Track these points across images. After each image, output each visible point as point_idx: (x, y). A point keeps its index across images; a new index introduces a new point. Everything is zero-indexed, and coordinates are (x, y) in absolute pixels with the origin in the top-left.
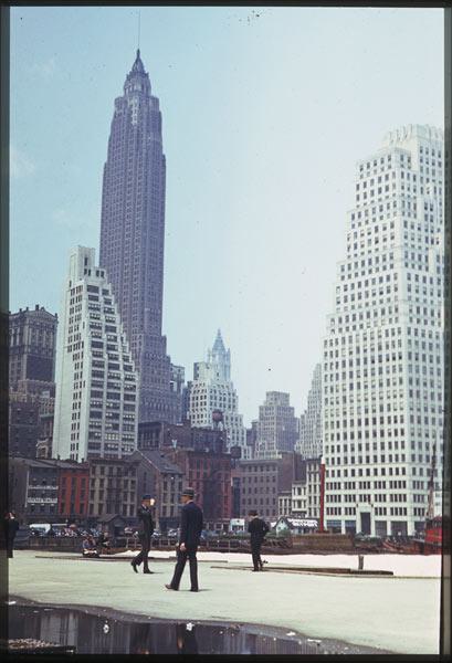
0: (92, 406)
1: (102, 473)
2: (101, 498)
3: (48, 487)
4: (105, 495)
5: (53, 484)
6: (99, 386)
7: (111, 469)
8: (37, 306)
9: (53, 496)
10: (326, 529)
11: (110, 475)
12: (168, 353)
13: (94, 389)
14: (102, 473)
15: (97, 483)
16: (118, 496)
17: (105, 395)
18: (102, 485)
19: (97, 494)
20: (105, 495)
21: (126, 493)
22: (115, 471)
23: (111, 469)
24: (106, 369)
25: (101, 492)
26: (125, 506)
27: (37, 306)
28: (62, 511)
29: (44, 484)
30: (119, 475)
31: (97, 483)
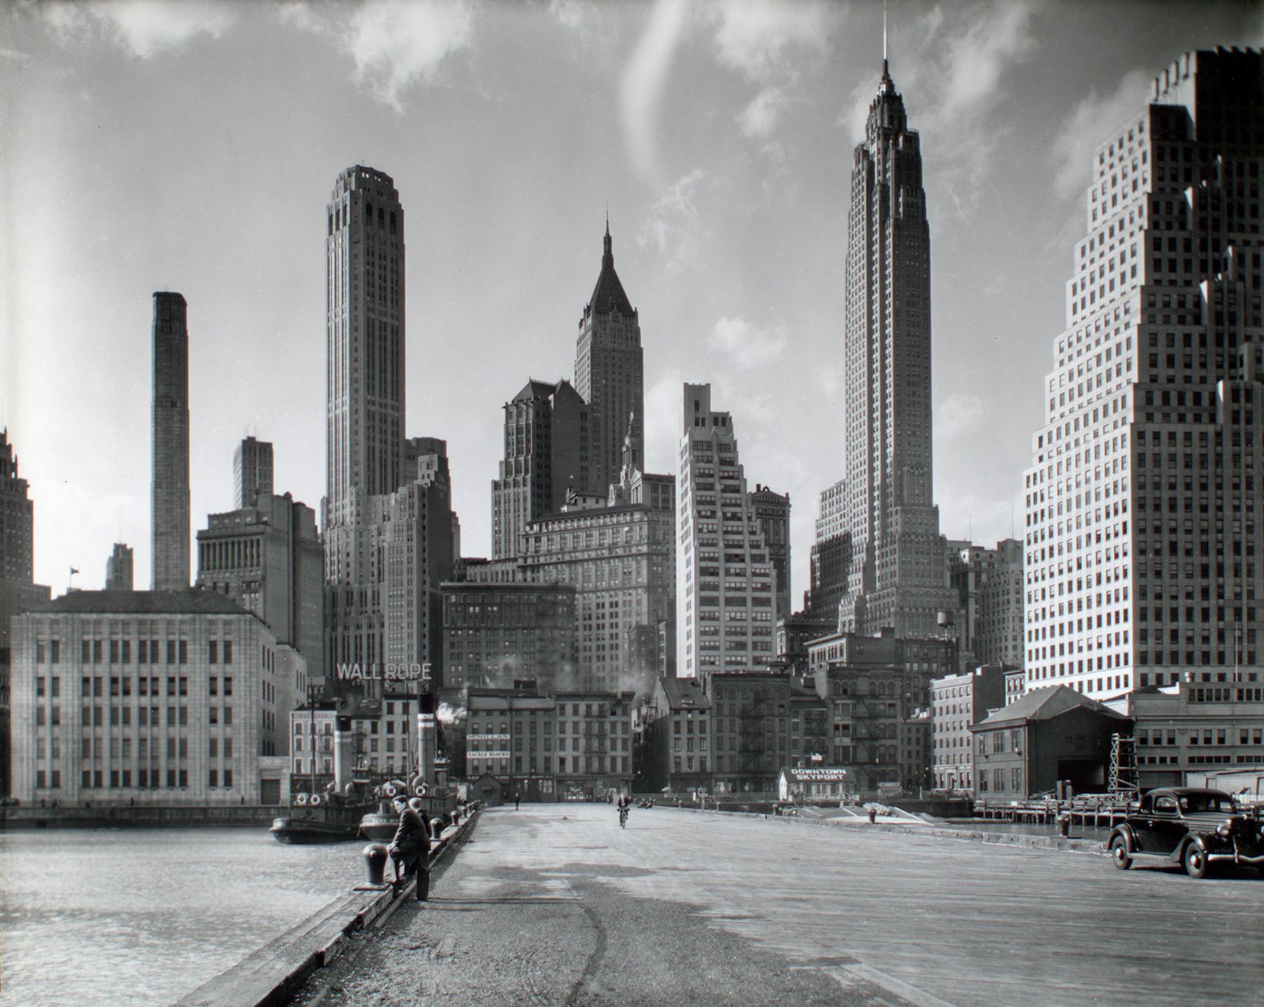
0: (703, 633)
1: (576, 712)
2: (575, 748)
3: (496, 736)
4: (582, 743)
5: (503, 731)
6: (712, 574)
7: (589, 707)
8: (758, 486)
9: (503, 747)
10: (709, 770)
11: (588, 714)
12: (935, 502)
13: (704, 594)
14: (576, 712)
15: (569, 728)
16: (601, 744)
17: (722, 601)
18: (576, 731)
19: (569, 743)
20: (582, 743)
21: (614, 741)
22: (595, 708)
23: (589, 707)
24: (720, 535)
25: (576, 741)
26: (614, 759)
27: (758, 486)
28: (519, 768)
29: (489, 731)
30: (601, 715)
31: (569, 728)
